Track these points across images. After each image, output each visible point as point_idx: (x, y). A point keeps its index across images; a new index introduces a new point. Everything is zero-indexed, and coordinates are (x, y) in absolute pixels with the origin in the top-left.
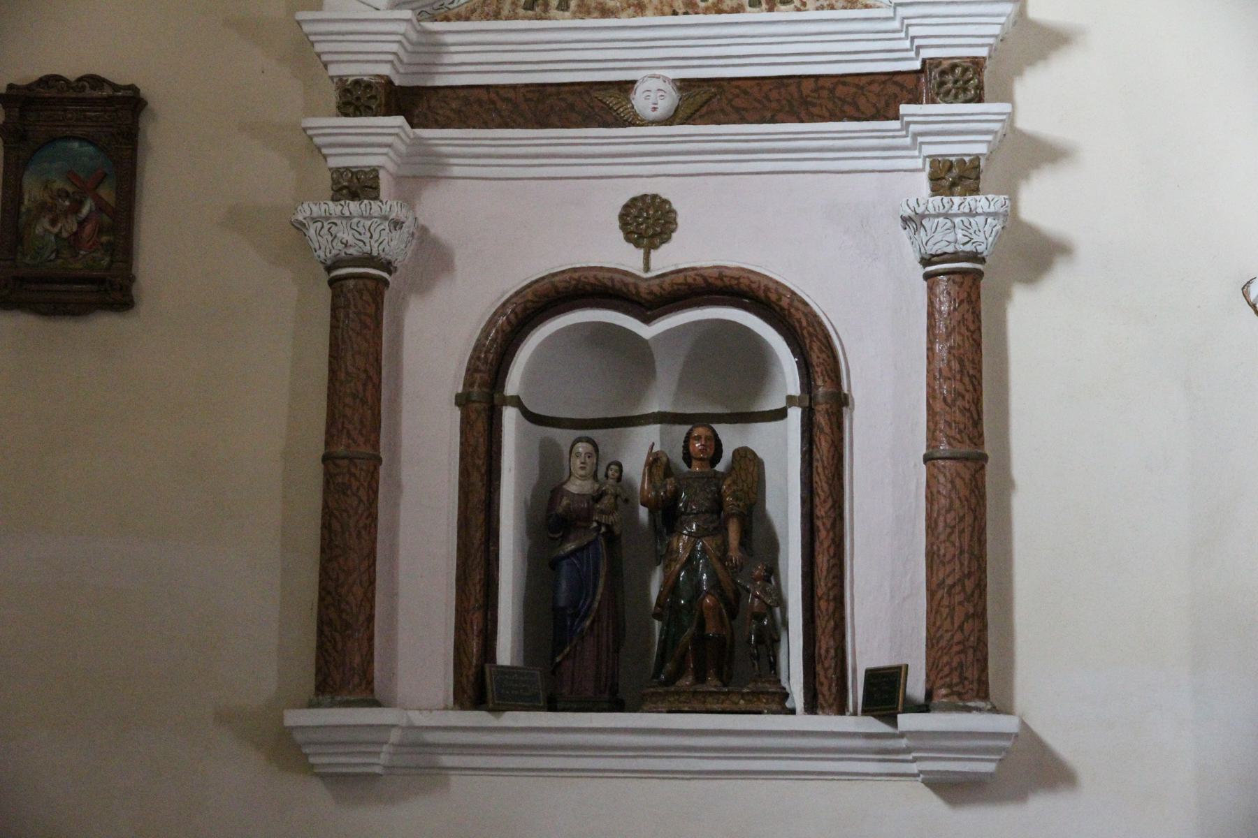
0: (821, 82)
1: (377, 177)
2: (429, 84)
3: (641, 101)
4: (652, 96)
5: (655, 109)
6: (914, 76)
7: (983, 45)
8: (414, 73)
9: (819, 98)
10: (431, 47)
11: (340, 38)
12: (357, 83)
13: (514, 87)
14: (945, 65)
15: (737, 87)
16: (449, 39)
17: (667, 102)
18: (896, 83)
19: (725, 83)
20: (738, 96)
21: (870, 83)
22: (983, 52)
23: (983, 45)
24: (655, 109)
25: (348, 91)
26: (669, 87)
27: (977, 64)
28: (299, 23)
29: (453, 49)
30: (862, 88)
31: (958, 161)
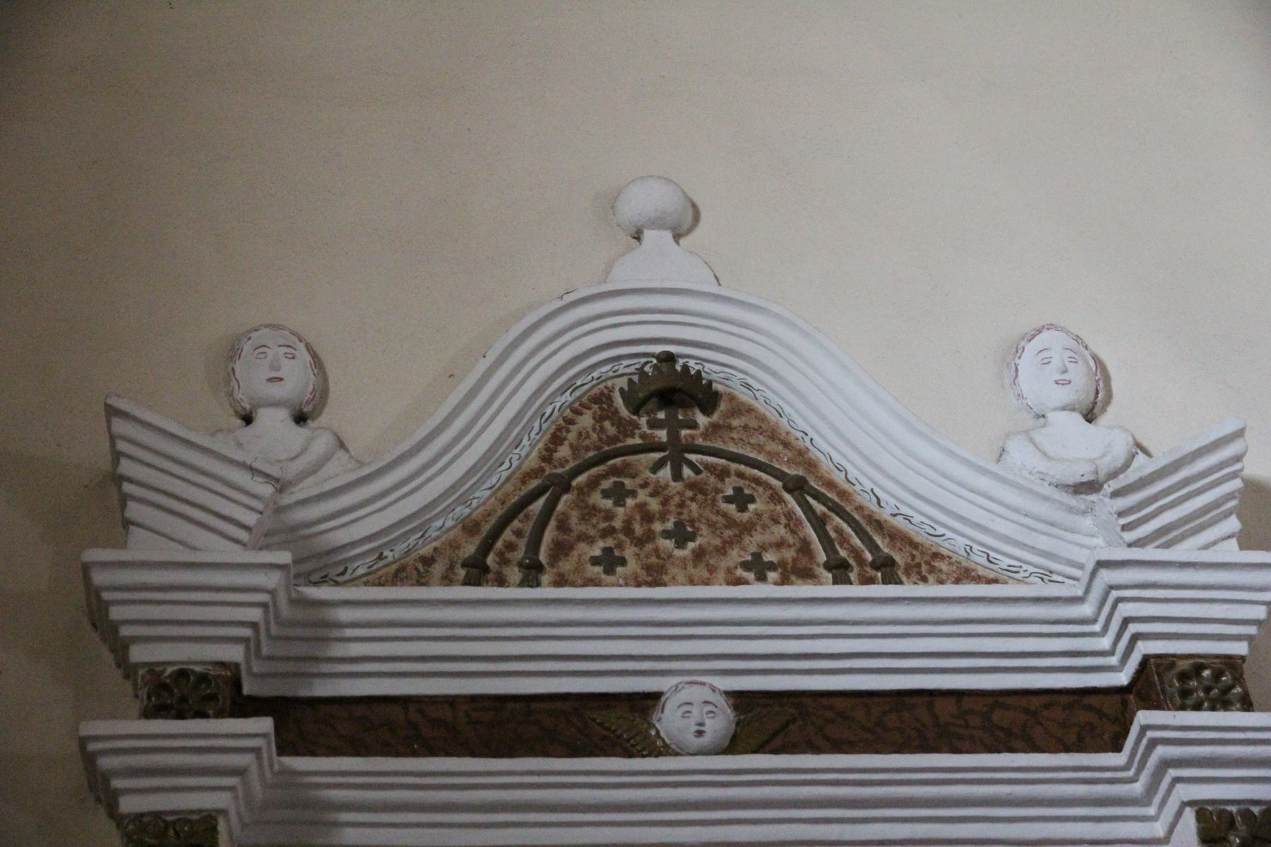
0: (967, 703)
1: (214, 830)
2: (304, 692)
3: (670, 721)
4: (693, 710)
5: (700, 733)
6: (1117, 698)
7: (1238, 638)
8: (274, 675)
9: (967, 726)
10: (317, 627)
11: (159, 596)
12: (182, 674)
13: (451, 701)
14: (1183, 665)
15: (831, 708)
16: (344, 615)
17: (720, 723)
18: (1090, 708)
19: (808, 701)
20: (829, 721)
21: (1046, 707)
22: (1241, 649)
23: (1238, 638)
24: (700, 733)
25: (164, 686)
26: (721, 701)
27: (1231, 664)
28: (86, 569)
29: (349, 632)
30: (1034, 714)
31: (1241, 813)
